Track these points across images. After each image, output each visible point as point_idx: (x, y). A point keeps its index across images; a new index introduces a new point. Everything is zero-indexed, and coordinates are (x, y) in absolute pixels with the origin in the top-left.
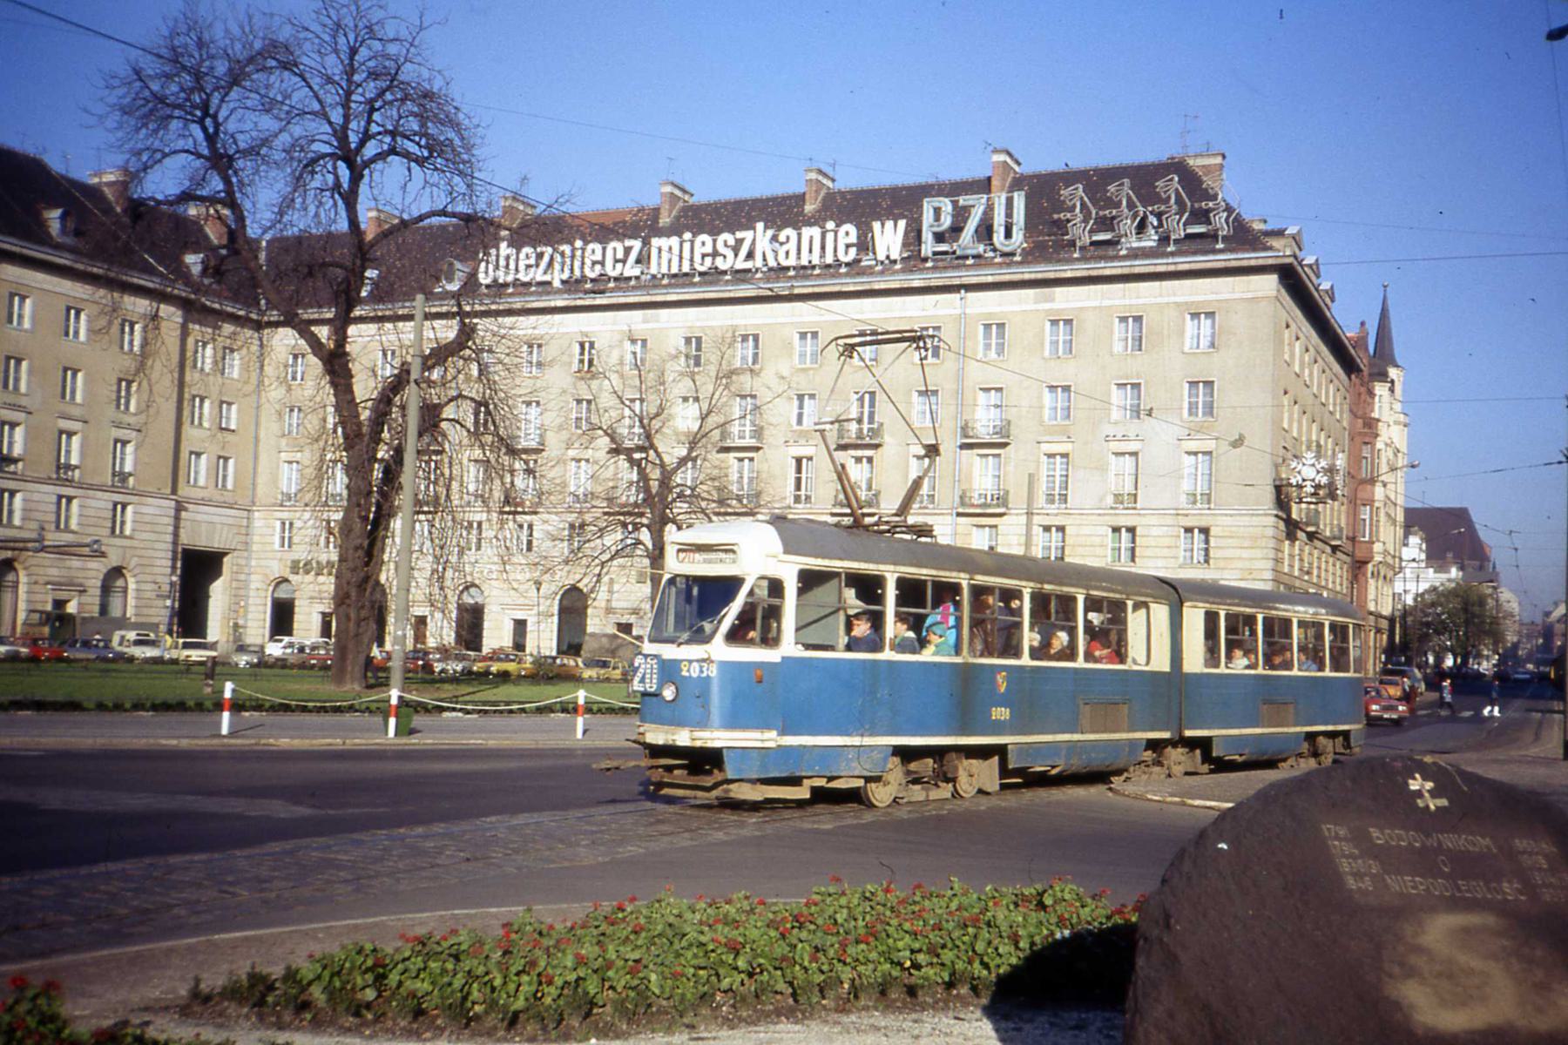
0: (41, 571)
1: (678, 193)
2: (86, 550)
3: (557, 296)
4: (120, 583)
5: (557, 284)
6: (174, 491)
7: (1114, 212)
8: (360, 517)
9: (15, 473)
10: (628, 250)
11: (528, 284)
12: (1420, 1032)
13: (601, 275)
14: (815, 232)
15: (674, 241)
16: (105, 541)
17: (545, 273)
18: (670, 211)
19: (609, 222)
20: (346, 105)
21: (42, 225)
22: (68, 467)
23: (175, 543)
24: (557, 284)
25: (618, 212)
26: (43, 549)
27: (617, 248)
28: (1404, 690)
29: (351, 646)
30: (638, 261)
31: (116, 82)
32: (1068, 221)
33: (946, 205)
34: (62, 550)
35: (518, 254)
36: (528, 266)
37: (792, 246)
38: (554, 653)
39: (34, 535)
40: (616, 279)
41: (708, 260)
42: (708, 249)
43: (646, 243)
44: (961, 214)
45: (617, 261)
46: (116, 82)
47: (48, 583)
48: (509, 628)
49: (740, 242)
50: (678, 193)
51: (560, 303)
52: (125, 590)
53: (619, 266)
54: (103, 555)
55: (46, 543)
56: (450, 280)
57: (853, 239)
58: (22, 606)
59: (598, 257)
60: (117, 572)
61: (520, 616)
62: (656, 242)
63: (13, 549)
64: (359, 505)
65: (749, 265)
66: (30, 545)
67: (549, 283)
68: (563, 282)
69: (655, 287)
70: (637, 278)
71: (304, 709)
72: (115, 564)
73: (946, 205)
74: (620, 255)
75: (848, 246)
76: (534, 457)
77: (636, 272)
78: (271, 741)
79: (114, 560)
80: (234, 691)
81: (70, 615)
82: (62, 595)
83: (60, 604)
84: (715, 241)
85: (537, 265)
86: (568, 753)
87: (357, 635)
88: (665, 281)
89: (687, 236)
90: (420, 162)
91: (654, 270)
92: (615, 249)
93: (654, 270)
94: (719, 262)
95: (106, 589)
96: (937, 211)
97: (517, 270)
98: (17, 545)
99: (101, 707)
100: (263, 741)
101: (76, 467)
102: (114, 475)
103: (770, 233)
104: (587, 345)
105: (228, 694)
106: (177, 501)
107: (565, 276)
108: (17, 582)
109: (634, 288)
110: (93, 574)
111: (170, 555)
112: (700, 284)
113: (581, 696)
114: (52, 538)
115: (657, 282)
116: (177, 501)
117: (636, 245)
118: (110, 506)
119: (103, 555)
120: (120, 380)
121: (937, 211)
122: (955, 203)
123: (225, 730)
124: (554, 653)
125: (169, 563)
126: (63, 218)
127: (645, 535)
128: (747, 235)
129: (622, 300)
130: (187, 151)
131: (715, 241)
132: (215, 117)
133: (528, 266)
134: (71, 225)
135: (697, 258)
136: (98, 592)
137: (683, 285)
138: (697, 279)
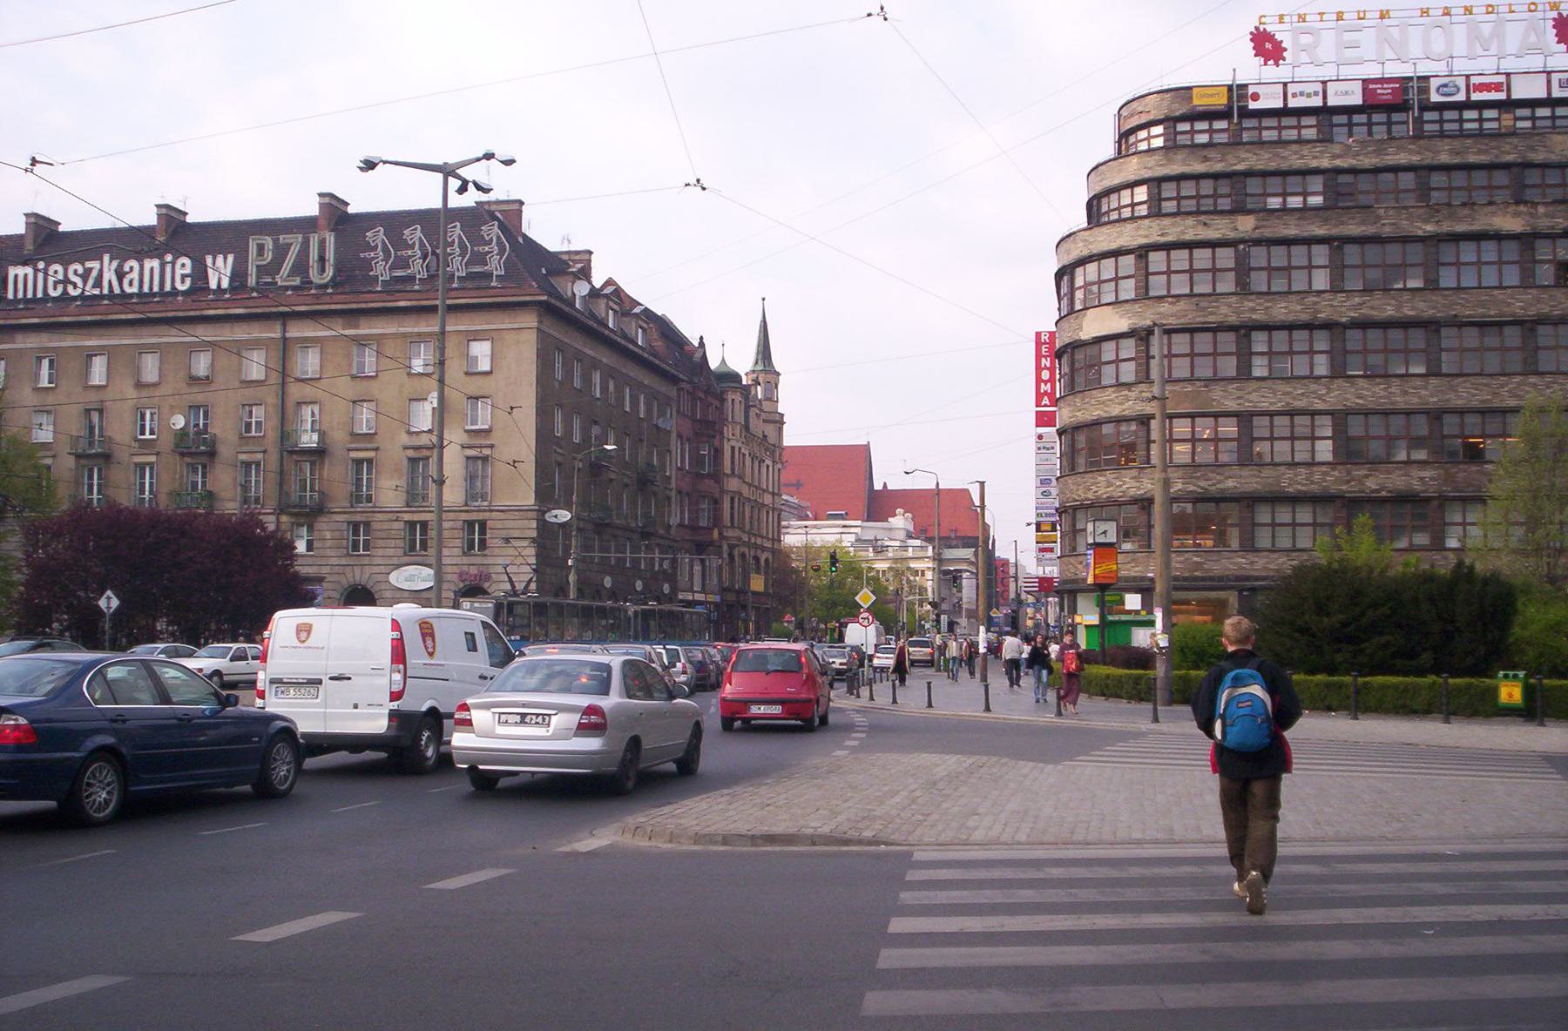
7: (487, 249)
14: (156, 263)
28: (311, 529)
32: (373, 258)
33: (269, 242)
37: (135, 275)
38: (1139, 608)
44: (281, 252)
49: (88, 271)
57: (188, 270)
65: (97, 292)
73: (269, 242)
75: (184, 277)
81: (750, 708)
84: (66, 271)
96: (261, 248)
103: (115, 264)
120: (88, 411)
121: (261, 248)
122: (276, 241)
124: (1139, 608)
128: (94, 265)
131: (66, 271)
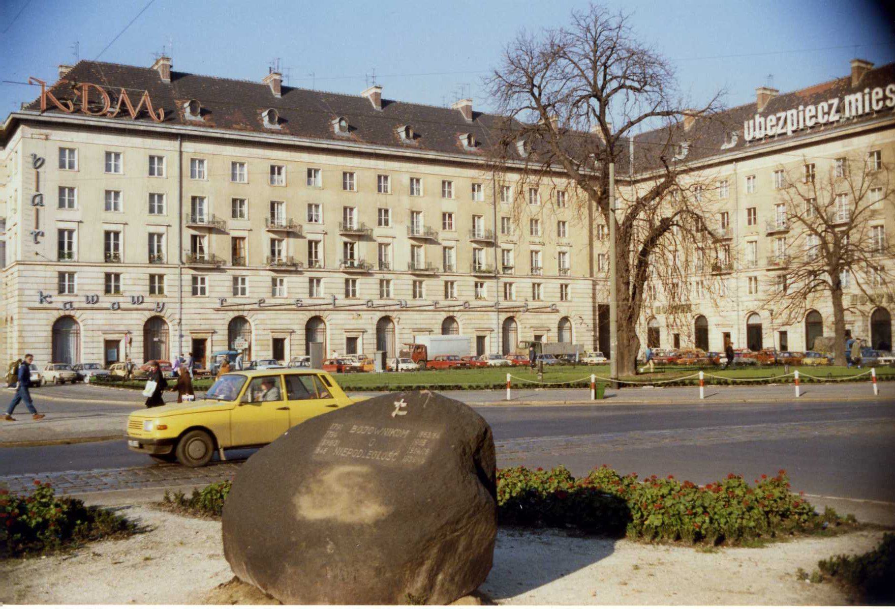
0: (528, 321)
1: (863, 65)
2: (549, 310)
3: (790, 141)
4: (568, 324)
5: (790, 133)
6: (592, 275)
8: (624, 283)
9: (511, 274)
10: (830, 106)
11: (773, 136)
12: (298, 518)
13: (816, 123)
15: (859, 95)
16: (558, 304)
17: (782, 128)
18: (858, 78)
19: (821, 91)
20: (594, 68)
21: (516, 150)
22: (537, 268)
23: (594, 302)
24: (790, 133)
25: (826, 84)
26: (527, 310)
27: (824, 105)
29: (626, 352)
30: (838, 111)
31: (487, 81)
34: (537, 310)
35: (766, 121)
36: (772, 126)
39: (522, 304)
40: (825, 124)
41: (881, 103)
42: (881, 95)
43: (842, 100)
45: (824, 114)
46: (487, 81)
47: (531, 327)
48: (777, 335)
50: (863, 65)
51: (791, 144)
52: (571, 329)
53: (826, 116)
54: (557, 311)
55: (529, 307)
56: (729, 141)
58: (397, 341)
59: (813, 113)
60: (565, 319)
61: (726, 330)
62: (847, 98)
63: (513, 312)
64: (622, 277)
66: (521, 309)
67: (785, 134)
68: (794, 132)
69: (849, 125)
70: (838, 121)
71: (568, 386)
72: (564, 316)
74: (826, 110)
76: (783, 236)
77: (837, 118)
78: (528, 402)
79: (563, 314)
80: (511, 378)
82: (538, 333)
83: (538, 337)
85: (777, 124)
86: (695, 406)
87: (629, 346)
88: (855, 120)
89: (867, 90)
90: (638, 90)
91: (847, 114)
92: (823, 107)
93: (847, 114)
94: (888, 103)
95: (560, 328)
97: (766, 129)
98: (515, 309)
99: (471, 387)
100: (525, 403)
101: (541, 268)
102: (560, 270)
104: (810, 166)
105: (508, 380)
106: (593, 281)
107: (795, 128)
108: (394, 328)
109: (836, 128)
110: (553, 321)
111: (591, 309)
112: (876, 118)
113: (796, 374)
114: (532, 304)
115: (850, 122)
116: (593, 281)
117: (835, 101)
118: (531, 285)
119: (557, 311)
123: (508, 398)
125: (592, 313)
126: (525, 144)
127: (827, 277)
129: (829, 136)
130: (528, 107)
131: (884, 91)
132: (539, 87)
133: (772, 126)
134: (529, 148)
135: (874, 102)
136: (556, 330)
137: (867, 121)
138: (875, 115)
